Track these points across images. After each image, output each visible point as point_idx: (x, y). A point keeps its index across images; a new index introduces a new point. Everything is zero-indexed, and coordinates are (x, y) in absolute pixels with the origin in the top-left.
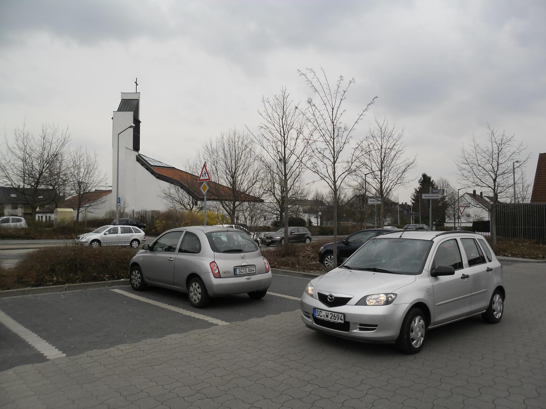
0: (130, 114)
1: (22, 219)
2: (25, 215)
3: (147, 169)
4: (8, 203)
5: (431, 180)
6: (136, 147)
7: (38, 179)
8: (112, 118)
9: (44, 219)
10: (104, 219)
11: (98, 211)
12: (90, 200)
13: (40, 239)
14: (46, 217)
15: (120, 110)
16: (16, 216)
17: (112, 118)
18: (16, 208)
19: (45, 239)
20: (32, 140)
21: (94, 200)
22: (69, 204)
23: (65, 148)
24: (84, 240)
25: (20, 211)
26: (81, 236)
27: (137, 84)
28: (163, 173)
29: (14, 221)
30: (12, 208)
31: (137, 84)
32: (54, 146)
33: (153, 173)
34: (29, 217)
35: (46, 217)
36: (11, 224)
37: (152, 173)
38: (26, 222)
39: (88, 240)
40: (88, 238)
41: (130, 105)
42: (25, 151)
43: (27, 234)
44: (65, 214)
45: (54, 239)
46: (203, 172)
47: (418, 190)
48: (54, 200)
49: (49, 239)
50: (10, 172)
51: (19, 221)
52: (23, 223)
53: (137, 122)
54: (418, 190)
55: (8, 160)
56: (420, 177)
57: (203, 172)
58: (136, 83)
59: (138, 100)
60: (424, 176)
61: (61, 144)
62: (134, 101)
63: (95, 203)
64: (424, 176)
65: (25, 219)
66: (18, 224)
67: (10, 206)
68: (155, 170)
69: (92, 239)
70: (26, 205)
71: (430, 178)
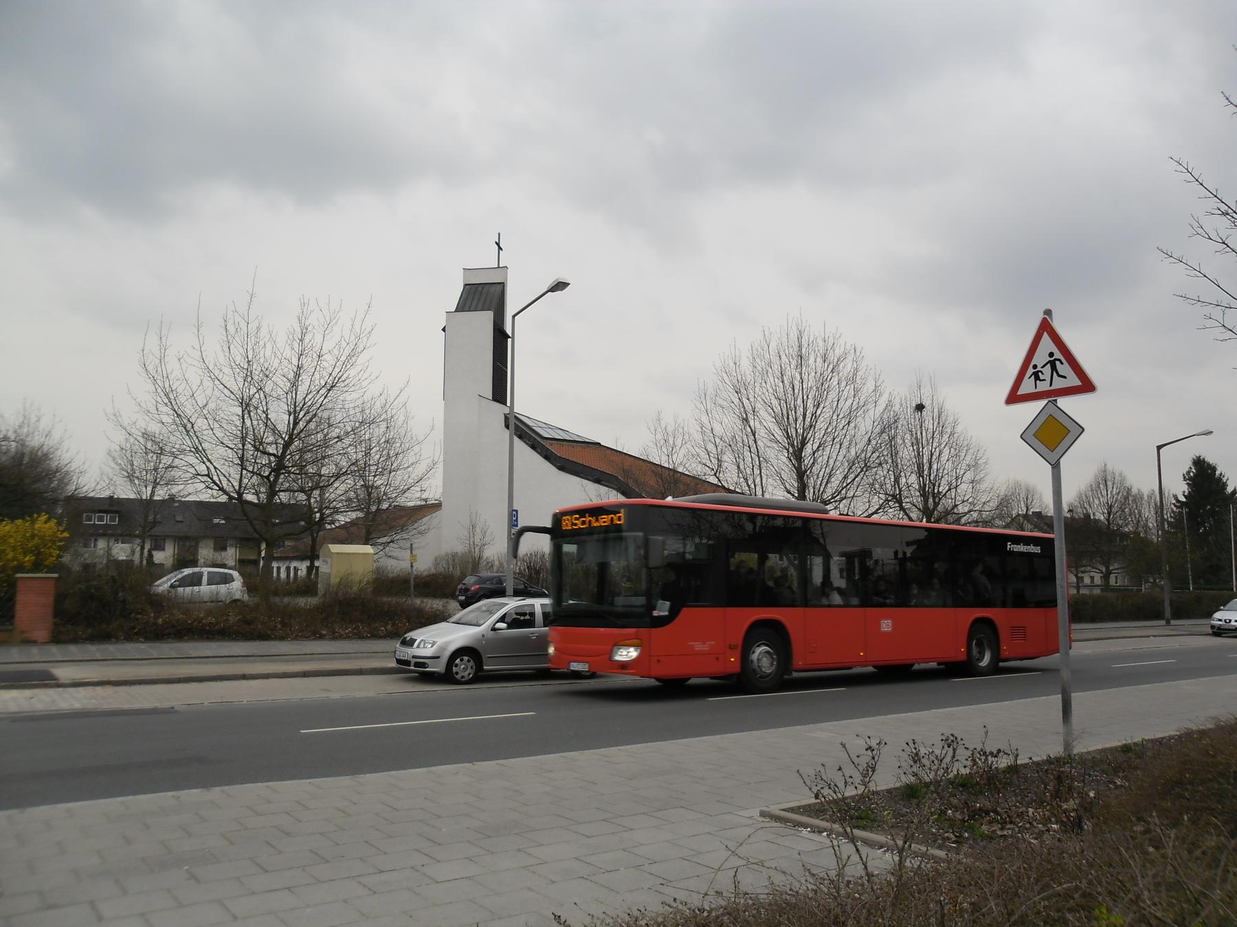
0: (487, 317)
1: (235, 574)
2: (242, 564)
3: (533, 447)
4: (205, 537)
5: (1218, 473)
6: (500, 392)
7: (280, 458)
8: (444, 330)
9: (283, 575)
10: (430, 576)
11: (421, 553)
12: (392, 528)
13: (282, 638)
14: (288, 569)
15: (461, 308)
16: (223, 566)
17: (444, 330)
18: (224, 549)
19: (296, 638)
20: (269, 346)
21: (403, 528)
22: (348, 534)
23: (352, 372)
24: (428, 651)
25: (231, 555)
26: (419, 635)
27: (500, 248)
28: (569, 456)
29: (214, 580)
30: (215, 549)
31: (500, 248)
32: (328, 361)
33: (548, 456)
34: (250, 569)
35: (288, 569)
36: (205, 589)
37: (547, 458)
38: (245, 584)
39: (442, 649)
40: (440, 641)
41: (484, 296)
42: (248, 376)
43: (248, 623)
44: (350, 560)
45: (322, 637)
46: (1040, 358)
47: (1183, 499)
48: (303, 529)
49: (307, 638)
50: (207, 435)
51: (227, 579)
52: (236, 586)
53: (501, 339)
54: (1183, 499)
55: (201, 400)
56: (1186, 465)
57: (1040, 358)
58: (498, 244)
59: (502, 285)
60: (1199, 463)
61: (347, 352)
62: (493, 288)
63: (405, 536)
64: (1199, 463)
65: (241, 574)
66: (223, 588)
67: (211, 543)
68: (554, 449)
69: (453, 647)
70: (246, 542)
71: (1214, 469)
